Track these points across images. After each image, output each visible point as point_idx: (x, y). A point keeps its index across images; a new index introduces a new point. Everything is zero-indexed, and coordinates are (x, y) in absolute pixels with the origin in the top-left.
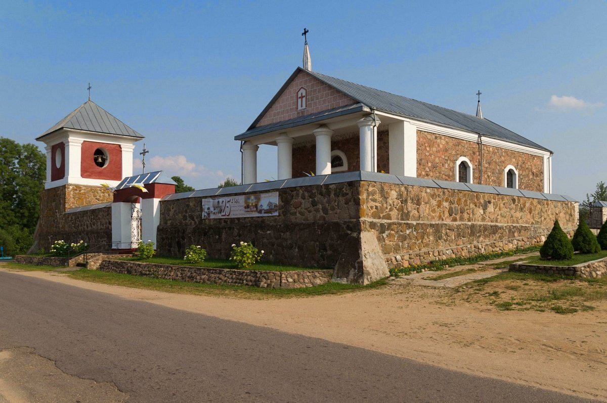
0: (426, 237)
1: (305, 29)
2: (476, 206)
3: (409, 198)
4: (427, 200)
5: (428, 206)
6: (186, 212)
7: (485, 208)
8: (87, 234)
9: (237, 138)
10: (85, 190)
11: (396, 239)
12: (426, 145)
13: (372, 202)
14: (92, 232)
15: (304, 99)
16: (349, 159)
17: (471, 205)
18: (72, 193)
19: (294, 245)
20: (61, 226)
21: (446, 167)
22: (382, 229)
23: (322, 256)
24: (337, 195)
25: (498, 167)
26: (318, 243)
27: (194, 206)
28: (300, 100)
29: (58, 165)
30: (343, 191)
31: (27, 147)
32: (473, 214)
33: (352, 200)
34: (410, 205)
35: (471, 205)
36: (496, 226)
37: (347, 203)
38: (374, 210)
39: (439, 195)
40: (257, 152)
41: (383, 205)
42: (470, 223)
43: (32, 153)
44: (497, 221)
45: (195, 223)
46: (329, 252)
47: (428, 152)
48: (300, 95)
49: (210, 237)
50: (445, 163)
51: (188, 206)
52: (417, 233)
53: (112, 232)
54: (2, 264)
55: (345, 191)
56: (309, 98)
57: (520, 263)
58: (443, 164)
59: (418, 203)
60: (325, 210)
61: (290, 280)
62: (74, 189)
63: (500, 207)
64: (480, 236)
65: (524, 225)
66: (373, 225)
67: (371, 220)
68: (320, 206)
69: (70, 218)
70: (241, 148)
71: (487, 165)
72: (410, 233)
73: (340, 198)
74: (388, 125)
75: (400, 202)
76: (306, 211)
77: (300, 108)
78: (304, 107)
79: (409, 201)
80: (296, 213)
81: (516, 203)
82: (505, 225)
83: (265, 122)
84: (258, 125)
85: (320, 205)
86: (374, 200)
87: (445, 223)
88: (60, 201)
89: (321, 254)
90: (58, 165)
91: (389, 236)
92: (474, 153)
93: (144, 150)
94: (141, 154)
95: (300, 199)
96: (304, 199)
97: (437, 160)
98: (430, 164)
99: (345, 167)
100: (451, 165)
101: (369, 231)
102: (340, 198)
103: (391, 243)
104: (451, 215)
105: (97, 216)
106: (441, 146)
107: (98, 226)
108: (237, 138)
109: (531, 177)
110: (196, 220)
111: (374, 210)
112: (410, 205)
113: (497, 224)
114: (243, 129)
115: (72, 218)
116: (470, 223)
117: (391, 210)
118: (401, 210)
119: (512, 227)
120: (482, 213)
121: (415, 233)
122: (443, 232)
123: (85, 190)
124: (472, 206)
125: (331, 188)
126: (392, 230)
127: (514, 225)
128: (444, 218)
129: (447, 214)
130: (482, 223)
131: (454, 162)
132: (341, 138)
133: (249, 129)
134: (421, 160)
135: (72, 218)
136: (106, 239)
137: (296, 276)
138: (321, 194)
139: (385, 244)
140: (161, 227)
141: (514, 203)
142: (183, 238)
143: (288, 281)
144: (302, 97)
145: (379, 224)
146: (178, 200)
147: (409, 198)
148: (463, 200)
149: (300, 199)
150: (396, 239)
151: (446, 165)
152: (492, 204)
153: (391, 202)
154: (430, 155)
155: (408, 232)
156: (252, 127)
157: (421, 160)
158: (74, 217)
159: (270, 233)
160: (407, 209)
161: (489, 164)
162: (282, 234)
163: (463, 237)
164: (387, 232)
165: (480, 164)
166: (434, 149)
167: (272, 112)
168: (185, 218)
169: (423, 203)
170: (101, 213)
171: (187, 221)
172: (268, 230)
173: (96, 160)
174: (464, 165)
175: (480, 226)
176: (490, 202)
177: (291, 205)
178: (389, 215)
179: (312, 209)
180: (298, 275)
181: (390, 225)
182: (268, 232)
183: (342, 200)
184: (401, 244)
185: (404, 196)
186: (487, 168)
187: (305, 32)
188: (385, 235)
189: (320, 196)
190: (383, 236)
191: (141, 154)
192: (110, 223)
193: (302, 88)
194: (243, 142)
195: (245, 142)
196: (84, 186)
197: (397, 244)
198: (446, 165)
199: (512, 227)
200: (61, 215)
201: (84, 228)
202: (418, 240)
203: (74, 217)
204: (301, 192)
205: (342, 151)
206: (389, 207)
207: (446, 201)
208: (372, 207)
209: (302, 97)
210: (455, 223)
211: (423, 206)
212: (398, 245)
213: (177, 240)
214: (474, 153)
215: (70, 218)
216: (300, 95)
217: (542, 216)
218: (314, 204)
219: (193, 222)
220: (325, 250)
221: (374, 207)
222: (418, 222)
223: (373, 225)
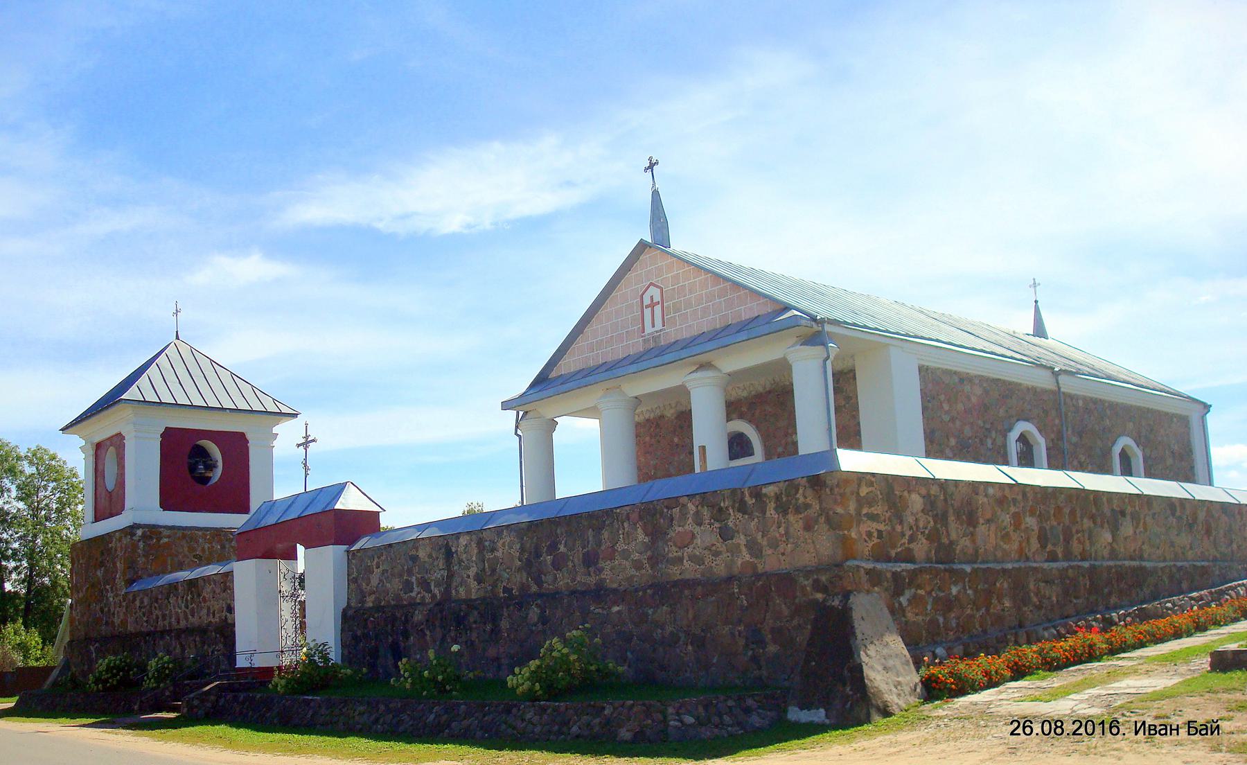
0: (994, 601)
1: (650, 159)
2: (1094, 523)
3: (951, 511)
4: (988, 516)
5: (993, 528)
6: (410, 572)
7: (1115, 529)
8: (178, 637)
9: (506, 405)
10: (169, 537)
11: (929, 607)
12: (942, 397)
13: (869, 522)
14: (189, 631)
15: (658, 309)
16: (766, 438)
17: (1085, 521)
18: (141, 545)
19: (682, 635)
20: (117, 621)
21: (989, 446)
22: (898, 584)
23: (754, 659)
24: (783, 509)
25: (1099, 443)
26: (741, 628)
27: (430, 556)
28: (648, 312)
29: (110, 483)
30: (797, 499)
31: (36, 457)
32: (1092, 544)
33: (822, 520)
34: (955, 529)
35: (1085, 521)
36: (1142, 568)
37: (808, 527)
38: (876, 541)
39: (1014, 500)
40: (556, 435)
41: (894, 529)
42: (1086, 564)
43: (49, 468)
44: (1141, 558)
45: (434, 596)
46: (772, 648)
47: (947, 413)
48: (647, 301)
49: (471, 629)
50: (986, 437)
51: (414, 559)
52: (976, 591)
53: (237, 629)
54: (1244, 736)
55: (801, 500)
56: (668, 307)
57: (1233, 646)
58: (981, 440)
59: (972, 521)
60: (753, 548)
61: (689, 720)
62: (144, 536)
63: (1145, 523)
64: (1110, 593)
65: (1198, 564)
66: (875, 577)
67: (870, 566)
68: (741, 540)
69: (138, 603)
70: (517, 427)
71: (1074, 439)
72: (959, 592)
73: (791, 518)
74: (852, 356)
75: (930, 519)
76: (706, 552)
77: (649, 329)
78: (659, 326)
79: (951, 518)
80: (680, 560)
81: (1178, 514)
82: (1162, 565)
83: (568, 365)
84: (553, 375)
85: (742, 537)
86: (873, 517)
87: (1035, 565)
88: (114, 564)
89: (750, 653)
90: (110, 483)
91: (914, 600)
92: (1046, 412)
93: (307, 437)
94: (299, 445)
95: (690, 526)
96: (700, 524)
97: (968, 431)
98: (953, 442)
99: (758, 456)
100: (999, 441)
101: (868, 592)
102: (791, 518)
103: (920, 618)
104: (1043, 546)
105: (199, 595)
106: (974, 400)
107: (202, 618)
108: (506, 405)
109: (1170, 462)
110: (436, 591)
111: (876, 541)
112: (955, 529)
113: (1144, 564)
114: (521, 385)
115: (142, 602)
116: (1086, 564)
117: (912, 539)
118: (933, 537)
119: (1174, 570)
120: (1110, 540)
121: (969, 592)
122: (1032, 586)
123: (169, 537)
124: (1087, 523)
125: (765, 495)
126: (919, 587)
127: (1179, 564)
128: (1030, 555)
129: (1035, 544)
130: (1111, 563)
131: (1004, 434)
132: (745, 394)
133: (533, 385)
134: (933, 432)
135: (142, 602)
136: (221, 646)
137: (701, 709)
138: (743, 508)
139: (906, 623)
140: (350, 613)
141: (1173, 515)
142: (406, 635)
143: (681, 721)
144: (652, 305)
145: (889, 575)
146: (390, 545)
147: (951, 511)
148: (1067, 511)
149: (690, 526)
150: (929, 607)
151: (989, 442)
152: (1128, 517)
153: (911, 520)
154: (953, 420)
155: (954, 590)
156: (541, 381)
157: (933, 432)
158: (146, 601)
159: (619, 612)
160: (948, 535)
161: (1080, 435)
162: (650, 612)
163: (1076, 598)
164: (908, 594)
165: (1060, 436)
166: (960, 407)
167: (581, 342)
168: (408, 586)
169: (981, 521)
170: (208, 588)
171: (413, 594)
172: (616, 603)
173: (192, 469)
174: (1023, 438)
175: (1110, 568)
176: (1123, 513)
177: (670, 540)
178: (909, 550)
179: (721, 546)
180: (706, 707)
181: (914, 574)
182: (615, 609)
183: (795, 522)
184: (941, 620)
185: (940, 504)
186: (1076, 445)
187: (651, 166)
188: (903, 600)
189: (739, 515)
190: (900, 604)
191: (299, 445)
192: (230, 609)
193: (651, 284)
194: (521, 413)
195: (526, 413)
196: (166, 527)
197: (931, 621)
198: (989, 442)
199: (1174, 570)
200: (117, 595)
201: (170, 623)
202: (978, 610)
203: (146, 601)
204: (691, 507)
205: (750, 422)
206: (908, 533)
207: (1032, 514)
208: (869, 534)
209: (652, 305)
210: (1054, 565)
211: (982, 529)
212: (933, 622)
213: (390, 639)
214: (1046, 412)
215: (138, 603)
216: (647, 301)
217: (1232, 542)
218: (725, 534)
219: (427, 596)
220: (762, 643)
221: (875, 534)
222: (976, 566)
223: (875, 577)
